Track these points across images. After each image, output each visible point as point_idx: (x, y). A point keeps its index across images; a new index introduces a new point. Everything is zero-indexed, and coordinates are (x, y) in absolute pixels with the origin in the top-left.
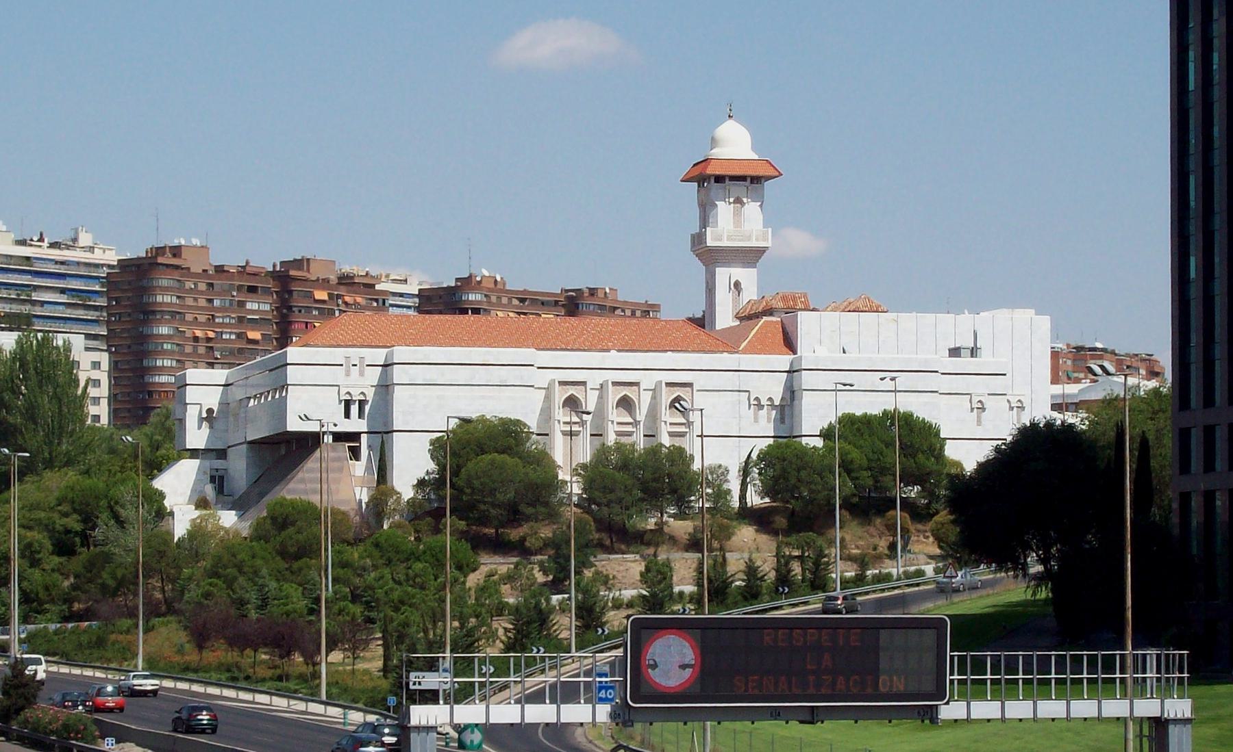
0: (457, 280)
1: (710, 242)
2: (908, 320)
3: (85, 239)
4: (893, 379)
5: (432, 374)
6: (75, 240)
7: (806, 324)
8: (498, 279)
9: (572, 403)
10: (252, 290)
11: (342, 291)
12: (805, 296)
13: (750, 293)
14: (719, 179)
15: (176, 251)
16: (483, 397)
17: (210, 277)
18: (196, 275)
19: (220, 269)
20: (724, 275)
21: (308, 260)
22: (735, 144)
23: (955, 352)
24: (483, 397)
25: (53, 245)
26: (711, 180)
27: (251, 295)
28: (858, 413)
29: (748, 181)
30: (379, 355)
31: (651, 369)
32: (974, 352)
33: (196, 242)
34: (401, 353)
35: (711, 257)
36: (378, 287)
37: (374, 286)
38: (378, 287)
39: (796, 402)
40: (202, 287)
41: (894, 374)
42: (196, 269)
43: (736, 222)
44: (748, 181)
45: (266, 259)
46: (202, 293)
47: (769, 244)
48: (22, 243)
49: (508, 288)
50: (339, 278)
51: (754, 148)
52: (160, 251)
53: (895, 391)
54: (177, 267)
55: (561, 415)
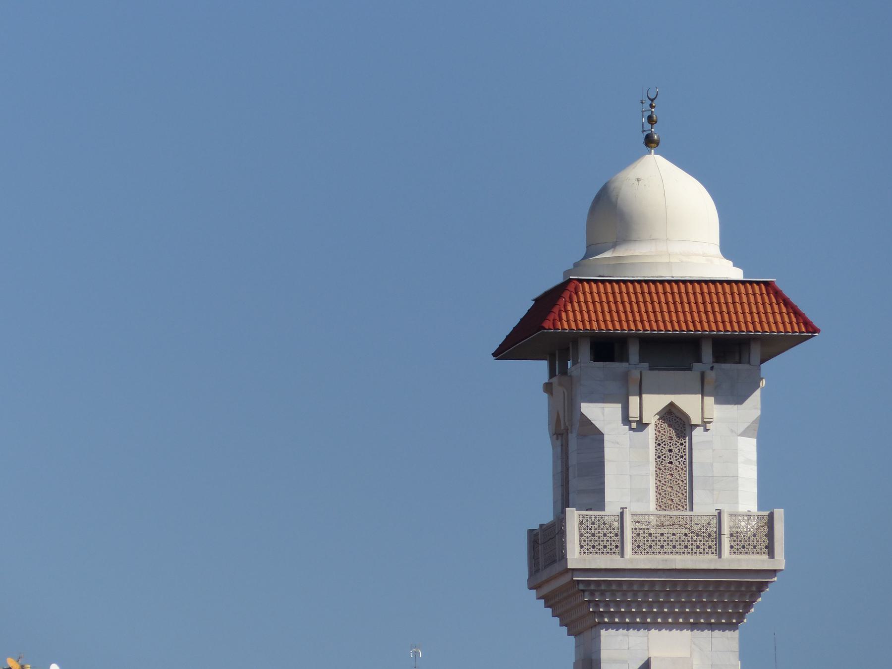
44: (705, 344)
51: (728, 249)
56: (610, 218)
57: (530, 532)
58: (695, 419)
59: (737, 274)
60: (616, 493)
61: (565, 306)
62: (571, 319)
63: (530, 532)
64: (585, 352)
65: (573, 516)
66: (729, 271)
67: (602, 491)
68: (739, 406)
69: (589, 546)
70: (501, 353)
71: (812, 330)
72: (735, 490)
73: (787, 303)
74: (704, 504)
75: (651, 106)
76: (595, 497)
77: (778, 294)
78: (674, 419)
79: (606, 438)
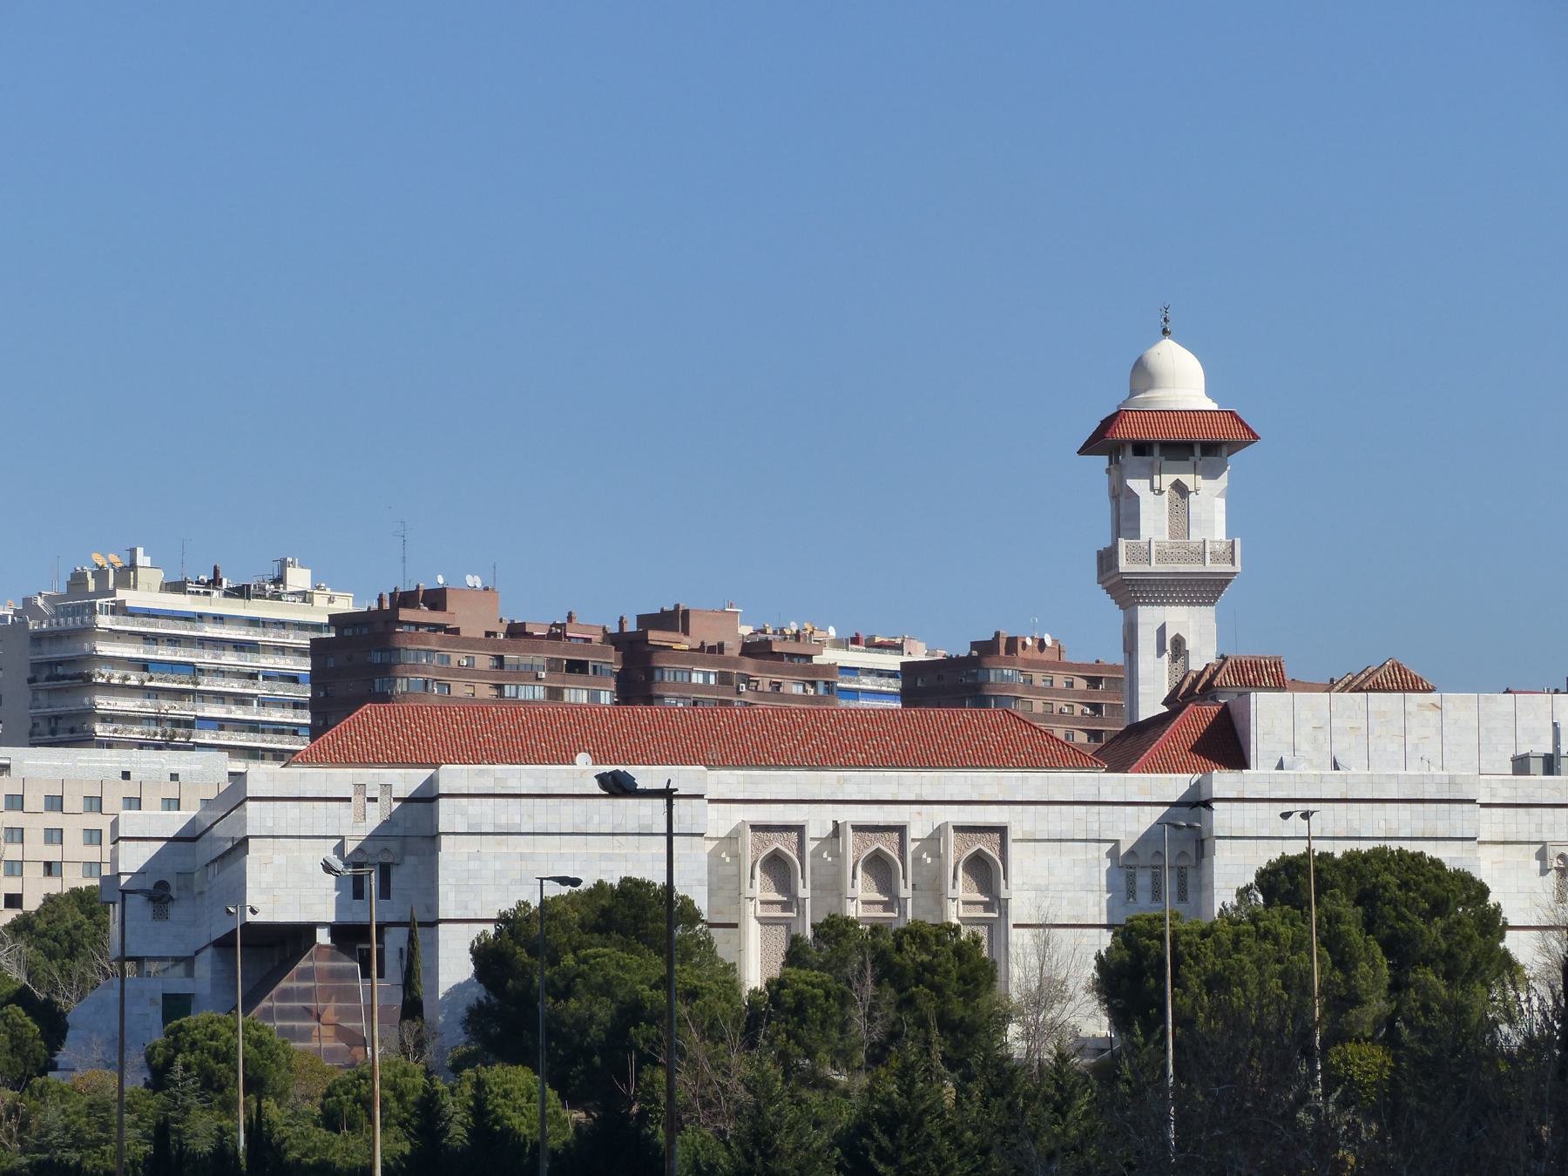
0: (974, 645)
1: (1124, 565)
2: (1460, 706)
3: (298, 578)
4: (1306, 815)
5: (509, 815)
6: (280, 580)
7: (1269, 715)
8: (1048, 642)
9: (777, 867)
10: (577, 667)
11: (749, 666)
12: (1278, 664)
13: (1202, 655)
14: (1142, 448)
15: (436, 599)
16: (603, 857)
17: (500, 646)
18: (471, 643)
19: (516, 631)
20: (1150, 617)
21: (686, 613)
22: (1183, 383)
23: (1521, 765)
24: (603, 857)
25: (241, 592)
26: (1134, 444)
27: (574, 676)
28: (613, 880)
29: (1196, 446)
30: (407, 780)
31: (929, 800)
32: (1550, 764)
33: (473, 581)
34: (453, 776)
35: (1129, 592)
36: (816, 660)
37: (809, 657)
38: (816, 660)
39: (1205, 861)
40: (484, 661)
41: (1311, 807)
42: (472, 629)
43: (1191, 518)
44: (1196, 446)
45: (603, 610)
46: (481, 674)
47: (1238, 568)
48: (177, 587)
49: (1066, 658)
50: (745, 645)
51: (1210, 392)
52: (406, 599)
53: (670, 835)
54: (438, 627)
55: (760, 889)
56: (1142, 375)
59: (1214, 407)
62: (1121, 432)
63: (600, 882)
64: (1129, 450)
65: (1122, 542)
69: (1132, 559)
70: (1082, 451)
74: (1196, 536)
76: (1135, 532)
77: (1237, 418)
78: (1179, 488)
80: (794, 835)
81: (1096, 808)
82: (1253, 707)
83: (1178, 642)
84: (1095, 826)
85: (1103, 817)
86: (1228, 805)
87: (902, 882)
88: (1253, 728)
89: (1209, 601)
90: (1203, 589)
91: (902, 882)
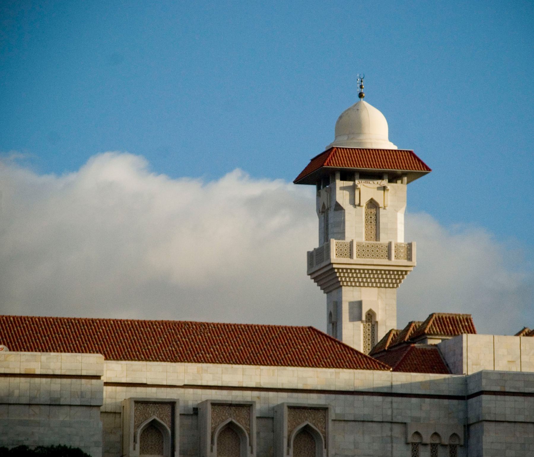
22: (377, 133)
44: (398, 167)
51: (391, 139)
56: (350, 123)
57: (308, 252)
58: (381, 205)
59: (395, 148)
60: (350, 235)
61: (332, 157)
62: (333, 164)
63: (308, 252)
64: (338, 175)
65: (333, 243)
66: (392, 146)
67: (344, 233)
68: (64, 442)
69: (340, 254)
70: (298, 181)
71: (429, 169)
72: (396, 234)
73: (419, 160)
74: (384, 239)
75: (362, 81)
76: (341, 235)
77: (415, 156)
78: (373, 204)
79: (346, 211)
80: (168, 409)
81: (389, 399)
82: (464, 344)
83: (371, 315)
84: (389, 412)
85: (395, 405)
86: (493, 397)
87: (249, 448)
88: (465, 360)
89: (395, 285)
90: (391, 278)
91: (249, 448)
